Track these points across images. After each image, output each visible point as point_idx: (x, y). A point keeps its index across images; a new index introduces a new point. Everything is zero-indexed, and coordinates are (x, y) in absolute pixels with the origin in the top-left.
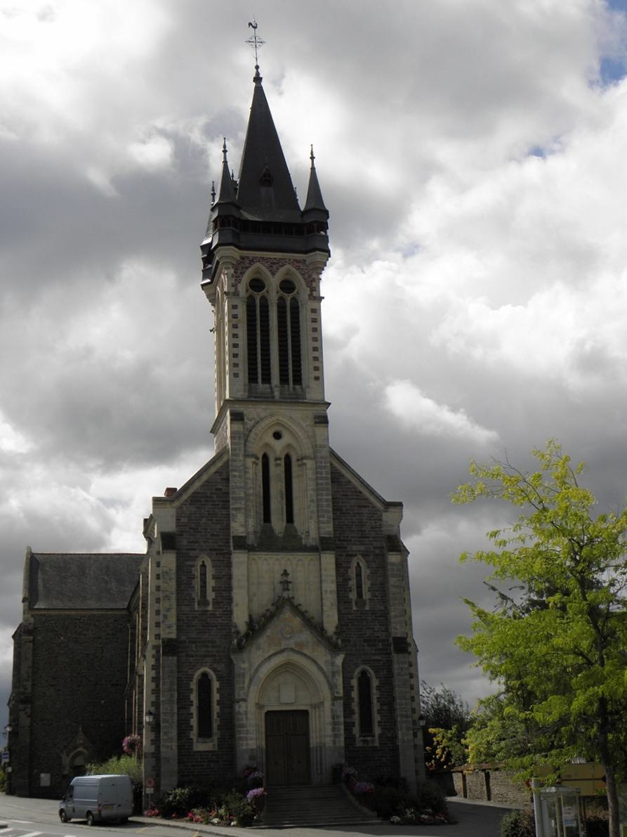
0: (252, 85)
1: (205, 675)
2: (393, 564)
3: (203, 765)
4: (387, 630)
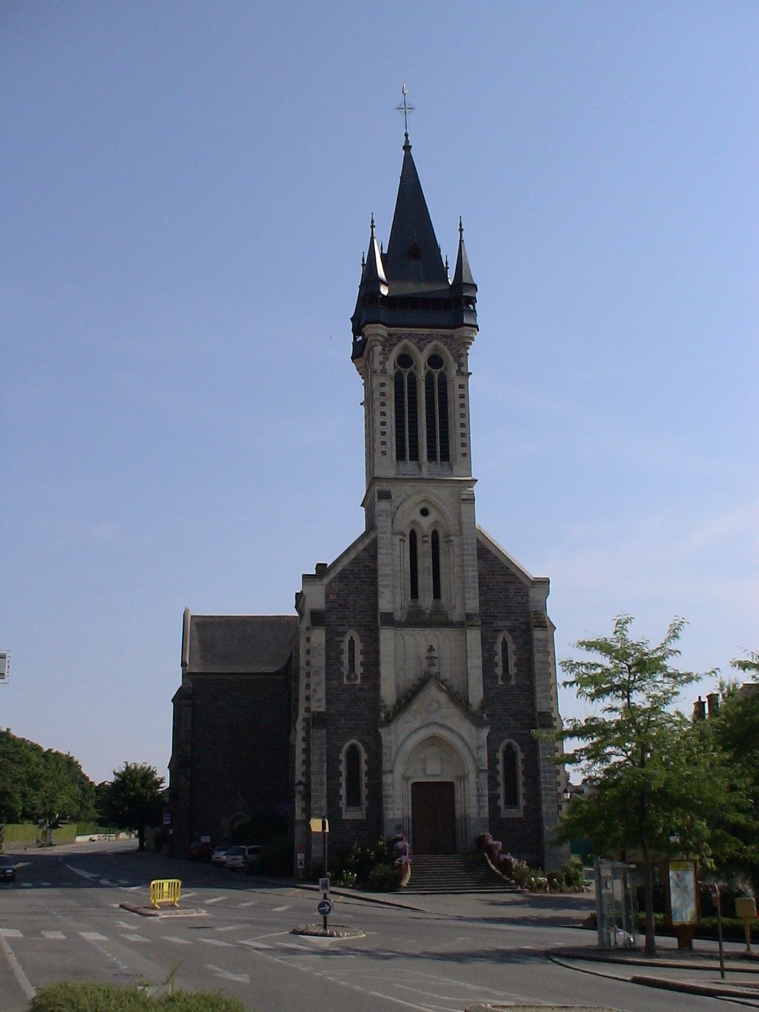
1: (353, 747)
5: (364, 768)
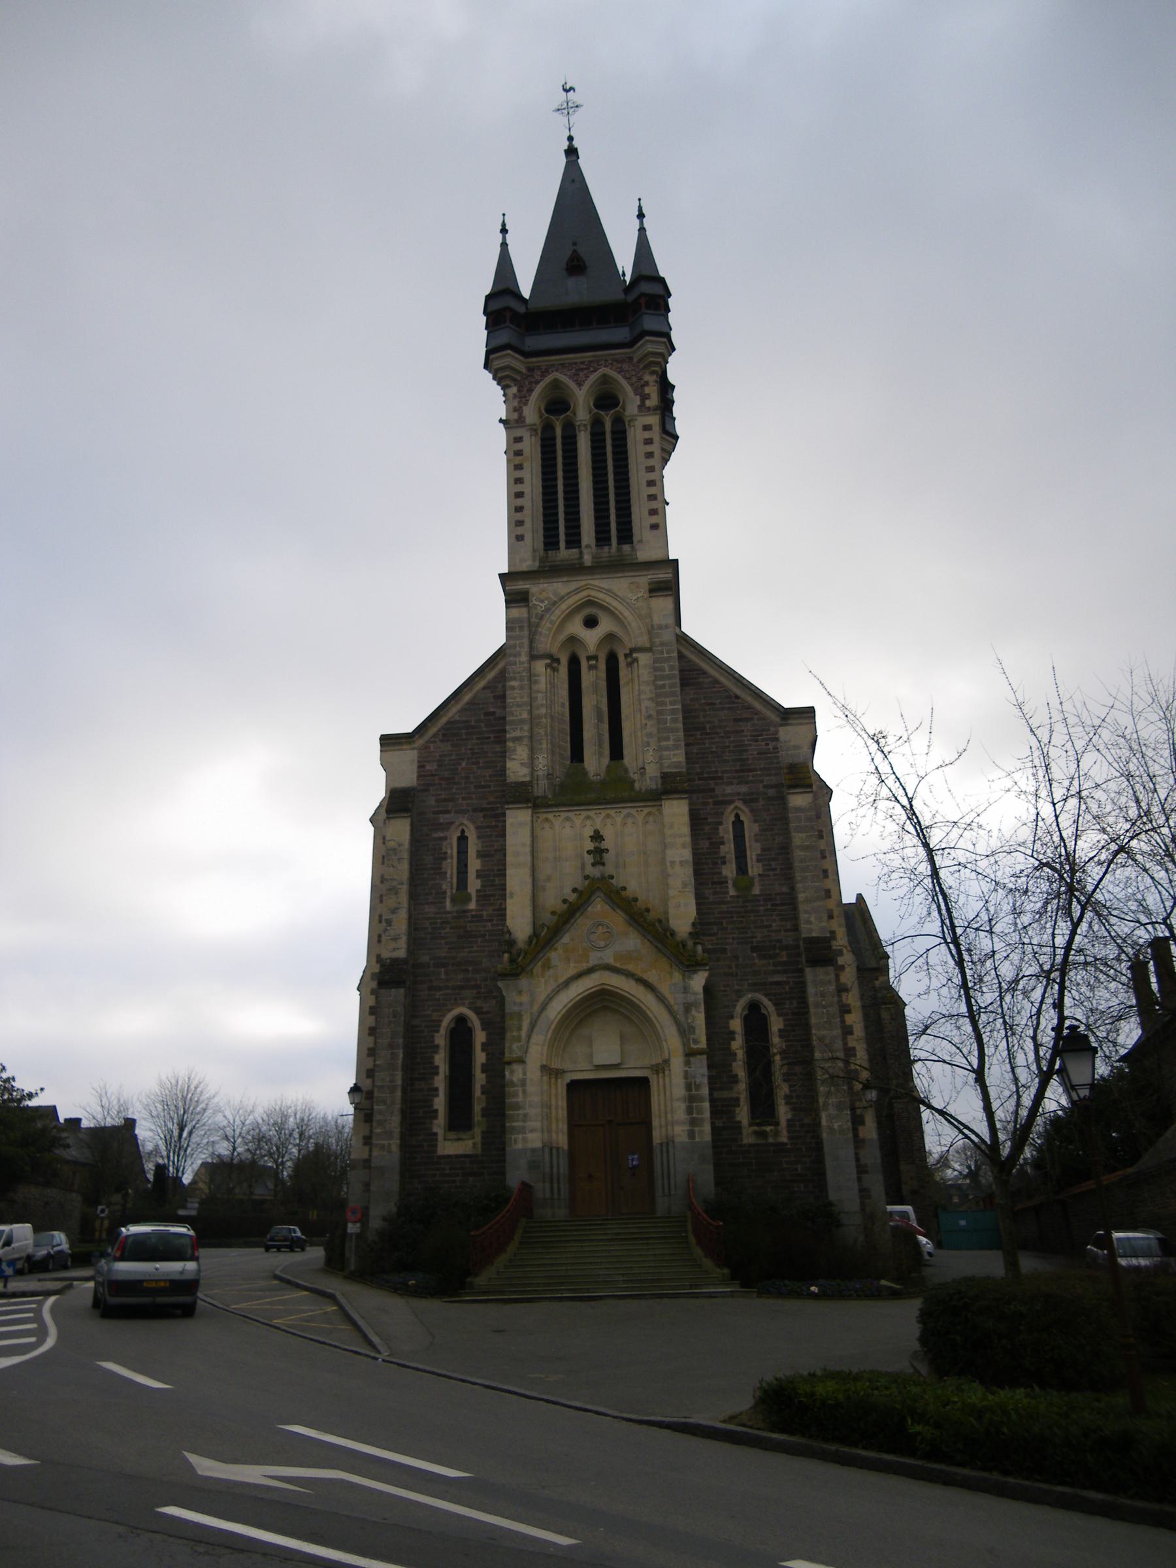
0: (560, 162)
1: (461, 1020)
2: (798, 809)
3: (454, 1182)
4: (796, 928)
5: (480, 1057)
